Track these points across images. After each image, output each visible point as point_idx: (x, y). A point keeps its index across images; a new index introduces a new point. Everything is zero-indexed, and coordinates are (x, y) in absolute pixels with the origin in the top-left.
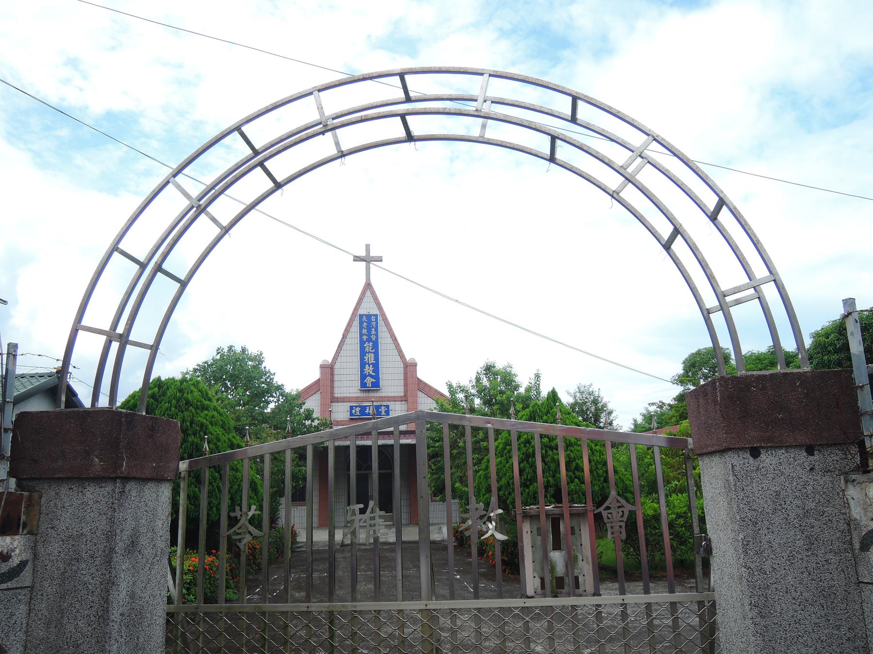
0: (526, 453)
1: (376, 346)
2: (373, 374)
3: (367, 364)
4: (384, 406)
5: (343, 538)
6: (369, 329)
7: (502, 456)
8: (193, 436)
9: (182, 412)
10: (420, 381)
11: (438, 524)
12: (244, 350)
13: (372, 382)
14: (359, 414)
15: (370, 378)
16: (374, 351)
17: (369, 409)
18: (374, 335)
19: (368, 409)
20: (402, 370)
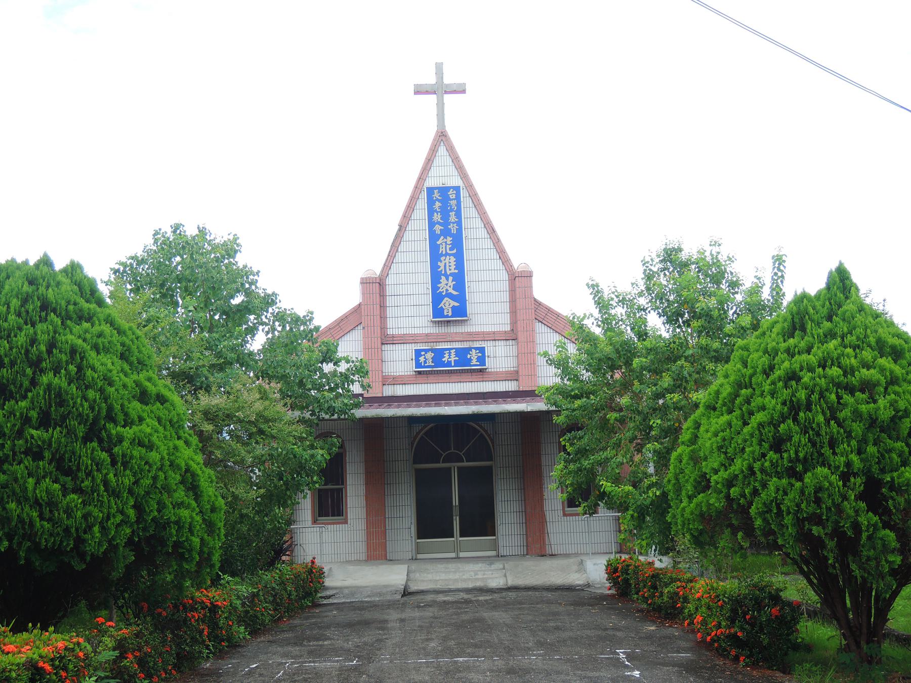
0: (791, 401)
1: (458, 243)
2: (455, 293)
3: (443, 275)
4: (476, 349)
5: (408, 580)
6: (445, 213)
7: (730, 412)
8: (51, 374)
9: (33, 325)
10: (538, 304)
11: (576, 555)
12: (202, 232)
13: (453, 307)
14: (430, 364)
15: (449, 300)
16: (455, 251)
17: (450, 355)
18: (453, 223)
19: (447, 356)
20: (505, 286)
